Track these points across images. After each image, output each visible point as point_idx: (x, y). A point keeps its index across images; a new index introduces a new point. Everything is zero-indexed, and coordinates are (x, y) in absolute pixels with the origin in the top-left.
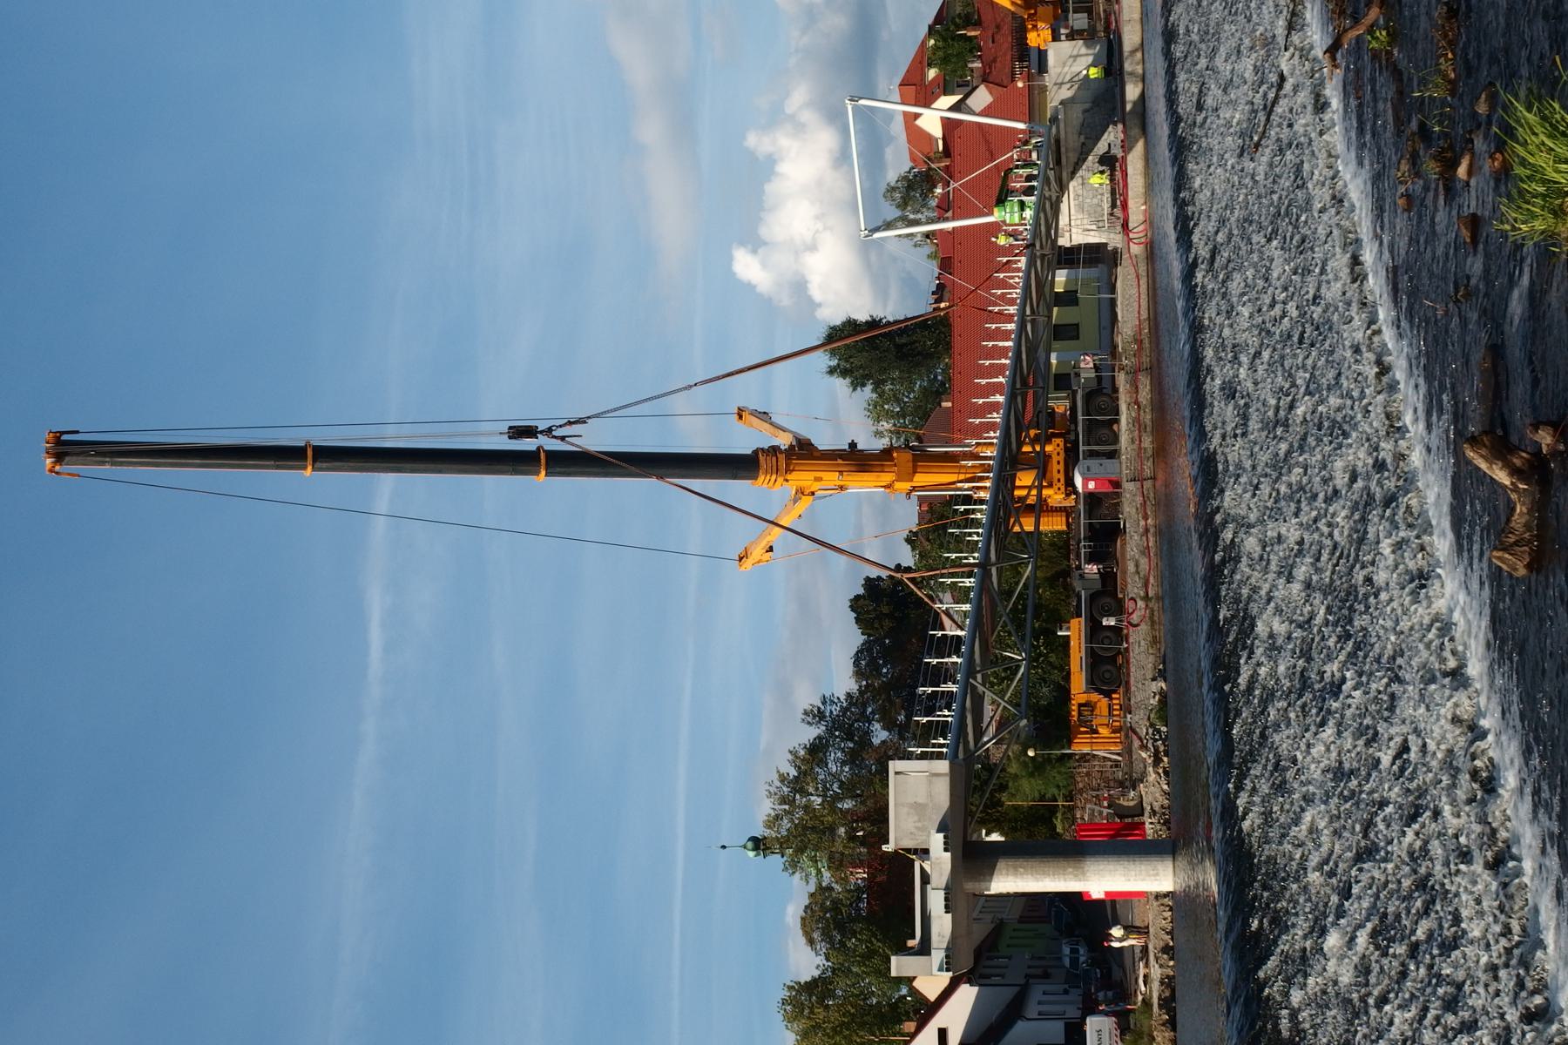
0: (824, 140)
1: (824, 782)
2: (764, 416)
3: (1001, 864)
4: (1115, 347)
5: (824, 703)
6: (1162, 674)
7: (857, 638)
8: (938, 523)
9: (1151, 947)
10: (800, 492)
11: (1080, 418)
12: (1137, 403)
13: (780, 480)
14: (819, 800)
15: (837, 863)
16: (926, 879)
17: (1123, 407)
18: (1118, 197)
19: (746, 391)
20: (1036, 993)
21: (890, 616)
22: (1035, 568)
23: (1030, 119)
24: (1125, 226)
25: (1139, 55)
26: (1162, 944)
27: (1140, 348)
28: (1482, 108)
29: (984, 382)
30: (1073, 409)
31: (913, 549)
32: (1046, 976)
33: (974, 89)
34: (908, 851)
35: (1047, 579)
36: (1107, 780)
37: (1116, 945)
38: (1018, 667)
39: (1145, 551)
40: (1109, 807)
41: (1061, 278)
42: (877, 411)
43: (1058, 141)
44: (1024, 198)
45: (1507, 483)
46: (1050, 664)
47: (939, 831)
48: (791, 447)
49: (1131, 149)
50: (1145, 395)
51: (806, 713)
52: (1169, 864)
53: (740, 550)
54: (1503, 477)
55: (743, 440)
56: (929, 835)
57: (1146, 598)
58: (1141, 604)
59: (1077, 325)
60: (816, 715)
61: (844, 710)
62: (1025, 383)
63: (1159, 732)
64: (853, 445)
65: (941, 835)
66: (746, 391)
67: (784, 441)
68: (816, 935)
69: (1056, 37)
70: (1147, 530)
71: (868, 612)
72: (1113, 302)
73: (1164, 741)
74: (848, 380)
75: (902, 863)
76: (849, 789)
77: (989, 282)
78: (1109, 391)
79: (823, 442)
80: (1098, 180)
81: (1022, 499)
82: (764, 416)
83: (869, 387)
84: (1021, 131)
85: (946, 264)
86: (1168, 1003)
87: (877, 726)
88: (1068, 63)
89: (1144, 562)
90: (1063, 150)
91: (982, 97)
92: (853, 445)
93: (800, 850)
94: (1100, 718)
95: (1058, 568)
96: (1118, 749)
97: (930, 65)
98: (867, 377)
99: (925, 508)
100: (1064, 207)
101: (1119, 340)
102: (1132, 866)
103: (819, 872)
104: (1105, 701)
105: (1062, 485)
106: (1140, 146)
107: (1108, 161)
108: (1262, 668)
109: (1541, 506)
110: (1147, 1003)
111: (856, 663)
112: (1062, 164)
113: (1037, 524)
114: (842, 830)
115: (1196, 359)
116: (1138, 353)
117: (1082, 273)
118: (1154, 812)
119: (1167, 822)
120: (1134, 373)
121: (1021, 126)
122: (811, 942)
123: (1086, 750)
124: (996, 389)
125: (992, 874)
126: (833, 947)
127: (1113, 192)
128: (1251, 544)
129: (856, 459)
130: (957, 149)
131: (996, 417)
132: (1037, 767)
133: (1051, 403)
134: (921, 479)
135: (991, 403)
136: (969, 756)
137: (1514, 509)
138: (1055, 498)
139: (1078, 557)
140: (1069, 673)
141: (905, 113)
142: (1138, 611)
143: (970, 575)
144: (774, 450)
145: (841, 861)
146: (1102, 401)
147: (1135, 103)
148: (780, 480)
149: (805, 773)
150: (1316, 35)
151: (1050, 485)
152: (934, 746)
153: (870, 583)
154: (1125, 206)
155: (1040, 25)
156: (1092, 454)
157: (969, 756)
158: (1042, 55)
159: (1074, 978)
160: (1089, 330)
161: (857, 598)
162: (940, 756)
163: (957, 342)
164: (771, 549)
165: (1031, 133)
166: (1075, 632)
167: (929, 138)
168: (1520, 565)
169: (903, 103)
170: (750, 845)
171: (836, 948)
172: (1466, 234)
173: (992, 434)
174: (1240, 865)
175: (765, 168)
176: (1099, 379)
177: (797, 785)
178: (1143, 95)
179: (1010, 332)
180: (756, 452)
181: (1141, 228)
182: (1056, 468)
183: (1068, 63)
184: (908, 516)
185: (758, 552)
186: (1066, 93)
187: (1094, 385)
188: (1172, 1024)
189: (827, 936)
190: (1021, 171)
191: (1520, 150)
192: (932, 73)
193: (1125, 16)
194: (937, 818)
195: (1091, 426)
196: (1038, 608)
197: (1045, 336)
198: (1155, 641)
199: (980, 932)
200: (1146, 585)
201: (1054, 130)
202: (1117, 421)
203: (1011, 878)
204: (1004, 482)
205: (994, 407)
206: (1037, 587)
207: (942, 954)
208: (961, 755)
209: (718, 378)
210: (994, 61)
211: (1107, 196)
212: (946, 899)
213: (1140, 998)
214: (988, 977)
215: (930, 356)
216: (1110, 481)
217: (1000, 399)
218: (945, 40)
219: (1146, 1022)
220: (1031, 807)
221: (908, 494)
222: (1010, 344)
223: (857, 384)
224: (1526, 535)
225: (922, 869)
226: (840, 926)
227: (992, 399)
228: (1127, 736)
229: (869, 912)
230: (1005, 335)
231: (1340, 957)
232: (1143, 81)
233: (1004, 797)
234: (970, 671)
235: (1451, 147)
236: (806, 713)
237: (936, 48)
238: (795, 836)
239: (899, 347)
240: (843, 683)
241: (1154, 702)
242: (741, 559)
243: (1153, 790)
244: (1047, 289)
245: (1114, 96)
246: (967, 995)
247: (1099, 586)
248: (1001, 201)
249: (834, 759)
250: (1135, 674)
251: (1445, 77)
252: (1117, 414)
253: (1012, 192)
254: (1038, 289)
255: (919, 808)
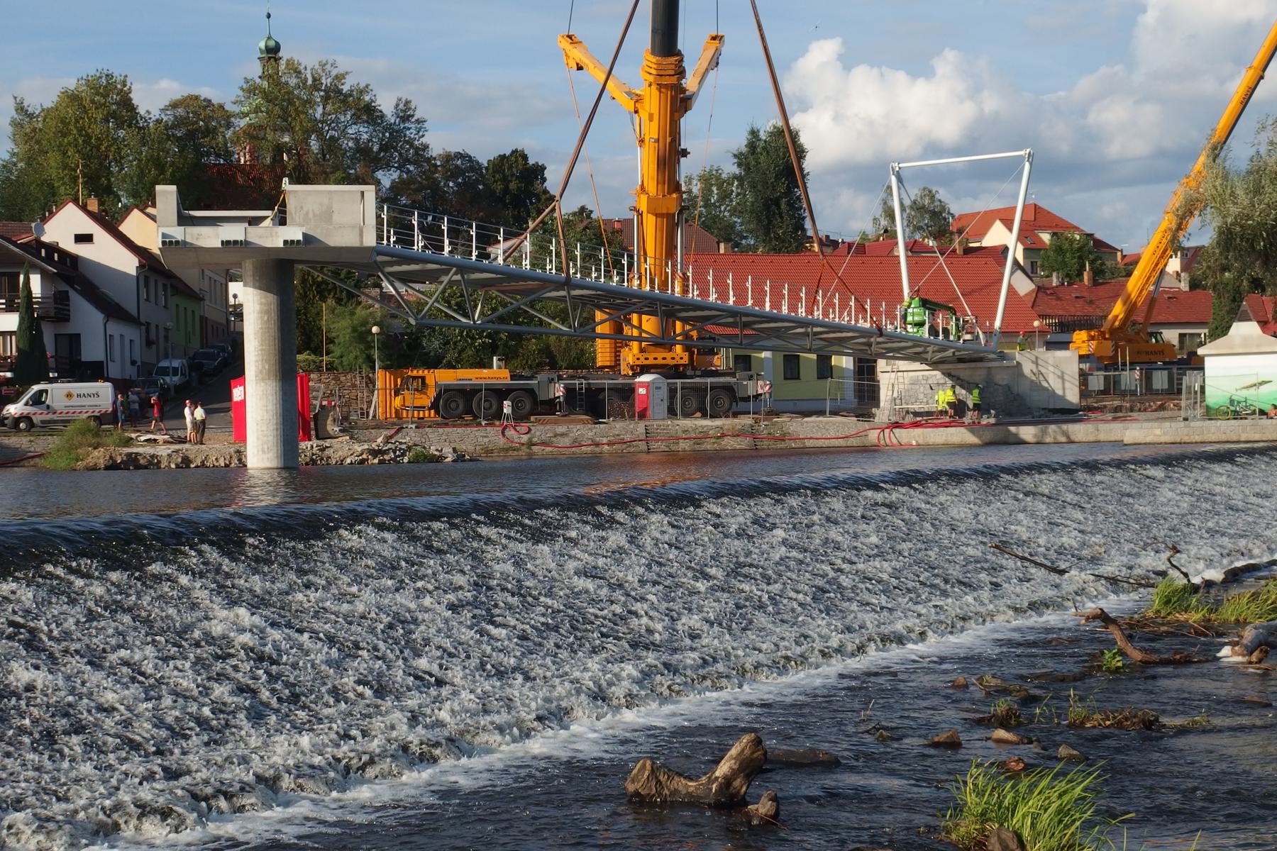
0: (949, 129)
1: (337, 121)
2: (715, 63)
3: (271, 298)
4: (778, 414)
5: (418, 121)
6: (460, 458)
7: (484, 156)
8: (605, 240)
9: (187, 446)
10: (638, 99)
11: (709, 380)
12: (723, 435)
13: (651, 79)
14: (318, 116)
15: (254, 134)
16: (254, 222)
17: (718, 422)
18: (924, 419)
19: (742, 42)
20: (131, 333)
21: (506, 190)
22: (560, 334)
23: (1004, 333)
24: (897, 425)
25: (1064, 439)
26: (192, 457)
27: (776, 439)
28: (1063, 751)
29: (749, 285)
30: (716, 374)
31: (574, 214)
32: (149, 343)
33: (1030, 278)
34: (284, 204)
35: (548, 346)
36: (348, 404)
37: (187, 411)
38: (466, 316)
39: (577, 443)
40: (322, 407)
41: (845, 362)
42: (710, 179)
43: (981, 360)
44: (927, 326)
45: (717, 774)
46: (463, 350)
47: (305, 235)
48: (684, 90)
49: (972, 431)
50: (730, 443)
51: (407, 103)
52: (274, 464)
53: (578, 37)
54: (723, 769)
55: (691, 38)
56: (301, 225)
57: (531, 444)
58: (525, 438)
59: (798, 378)
60: (405, 113)
61: (410, 143)
62: (746, 325)
63: (403, 455)
64: (685, 153)
65: (300, 238)
66: (742, 42)
67: (690, 83)
68: (181, 111)
69: (1082, 358)
70: (597, 445)
71: (510, 167)
72: (821, 413)
73: (394, 460)
74: (744, 150)
75: (273, 201)
76: (331, 146)
77: (846, 288)
78: (734, 408)
79: (688, 122)
80: (944, 397)
81: (629, 321)
82: (715, 63)
83: (736, 170)
84: (992, 324)
85: (860, 249)
86: (132, 462)
87: (395, 175)
88: (1058, 370)
89: (566, 441)
90: (973, 365)
91: (1025, 286)
92: (685, 153)
93: (266, 96)
94: (409, 397)
95: (559, 358)
96: (380, 415)
97: (1054, 234)
98: (748, 169)
99: (617, 226)
100: (917, 366)
101: (784, 419)
102: (272, 427)
103: (246, 115)
104: (428, 403)
105: (642, 362)
106: (973, 439)
107: (958, 408)
108: (502, 553)
109: (693, 803)
110: (129, 442)
111: (459, 155)
112: (957, 364)
113: (603, 336)
114: (286, 139)
115: (783, 490)
116: (771, 437)
117: (850, 382)
118: (323, 449)
119: (313, 462)
120: (752, 433)
121: (997, 324)
122: (174, 105)
123: (379, 384)
124: (741, 296)
125: (254, 287)
126: (167, 127)
127: (929, 413)
128: (616, 538)
129: (670, 155)
130: (970, 259)
131: (694, 294)
132: (362, 336)
133: (723, 351)
134: (650, 222)
135: (721, 290)
136: (380, 266)
137: (691, 780)
138: (626, 353)
139: (572, 377)
140: (454, 368)
141: (1014, 209)
142: (518, 435)
143: (559, 269)
144: (681, 73)
145: (257, 138)
146: (724, 401)
147: (1016, 435)
148: (651, 79)
149: (344, 102)
150: (1113, 603)
151: (642, 350)
152: (389, 232)
153: (539, 171)
154: (916, 425)
155: (1093, 344)
156: (672, 392)
157: (380, 266)
158: (1064, 345)
159: (148, 373)
160: (792, 389)
161: (525, 157)
162: (380, 238)
163: (783, 260)
164: (580, 68)
165: (989, 333)
166: (497, 373)
167: (982, 234)
168: (638, 786)
169: (1025, 206)
170: (272, 44)
171: (166, 130)
172: (942, 737)
173: (677, 289)
174: (274, 527)
175: (920, 68)
176: (747, 399)
177: (335, 95)
178: (1024, 442)
179: (780, 309)
180: (679, 54)
181: (895, 441)
182: (660, 356)
183: (1058, 370)
184: (607, 210)
185: (577, 54)
186: (1028, 368)
187: (740, 394)
188: (112, 466)
189: (179, 122)
190: (953, 323)
191: (1043, 784)
192: (1046, 237)
193: (1102, 426)
194: (318, 234)
195: (700, 391)
196: (517, 336)
197: (792, 345)
198: (488, 452)
199: (190, 277)
200: (544, 444)
201: (993, 356)
202: (704, 416)
203: (258, 307)
204: (649, 304)
205: (723, 295)
206: (538, 336)
207: (180, 238)
208: (380, 258)
209: (756, 16)
210: (1059, 299)
211: (926, 408)
212: (236, 242)
213: (133, 435)
214: (147, 286)
215: (767, 233)
216: (646, 409)
217: (713, 297)
218: (1080, 249)
219: (109, 440)
220: (320, 329)
221: (635, 209)
222: (768, 308)
223: (741, 159)
224: (666, 791)
225: (265, 218)
226: (191, 135)
227: (712, 289)
228: (394, 424)
229: (205, 161)
230: (776, 304)
231: (231, 622)
232: (1038, 443)
233: (331, 302)
234: (462, 269)
235: (1019, 724)
236: (407, 103)
237: (1072, 241)
238: (282, 94)
239: (777, 202)
240: (438, 141)
241: (433, 450)
242: (570, 37)
243: (344, 450)
244: (836, 348)
245: (1024, 415)
246: (128, 264)
247: (542, 397)
248: (925, 303)
249: (363, 132)
250: (456, 433)
251: (1087, 718)
252: (712, 417)
253: (933, 314)
254: (836, 339)
255: (327, 215)
